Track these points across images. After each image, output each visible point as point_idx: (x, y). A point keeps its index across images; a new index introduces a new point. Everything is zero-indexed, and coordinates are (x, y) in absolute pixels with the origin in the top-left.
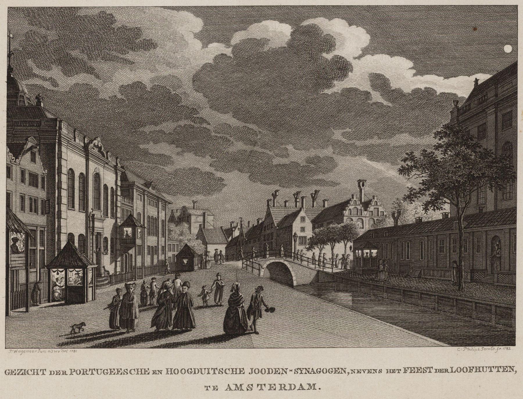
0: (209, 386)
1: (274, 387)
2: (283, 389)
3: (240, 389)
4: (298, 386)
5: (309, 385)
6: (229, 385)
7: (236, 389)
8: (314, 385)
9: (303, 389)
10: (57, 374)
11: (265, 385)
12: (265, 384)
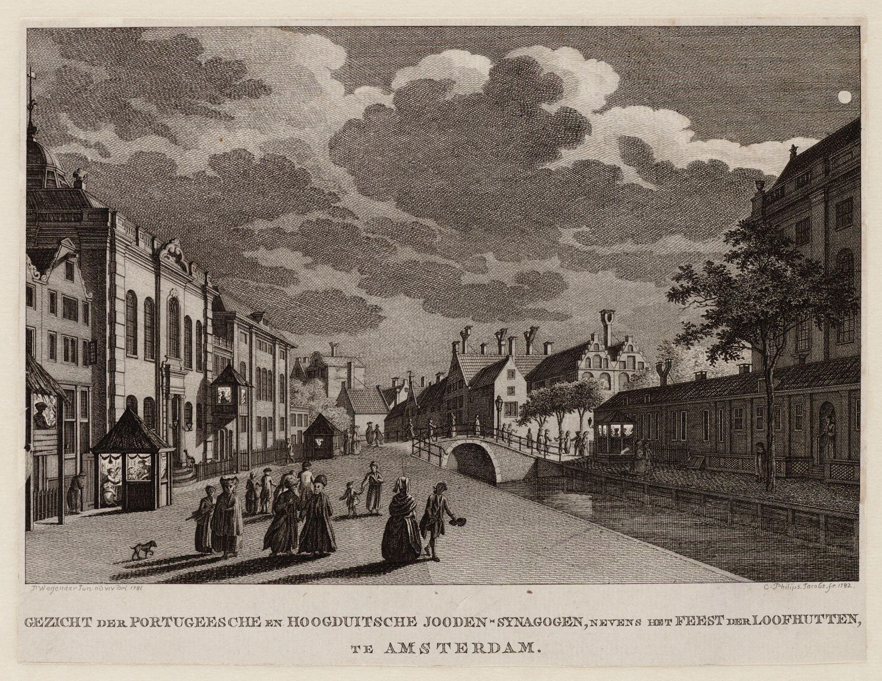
0: (359, 647)
5: (523, 644)
10: (109, 626)
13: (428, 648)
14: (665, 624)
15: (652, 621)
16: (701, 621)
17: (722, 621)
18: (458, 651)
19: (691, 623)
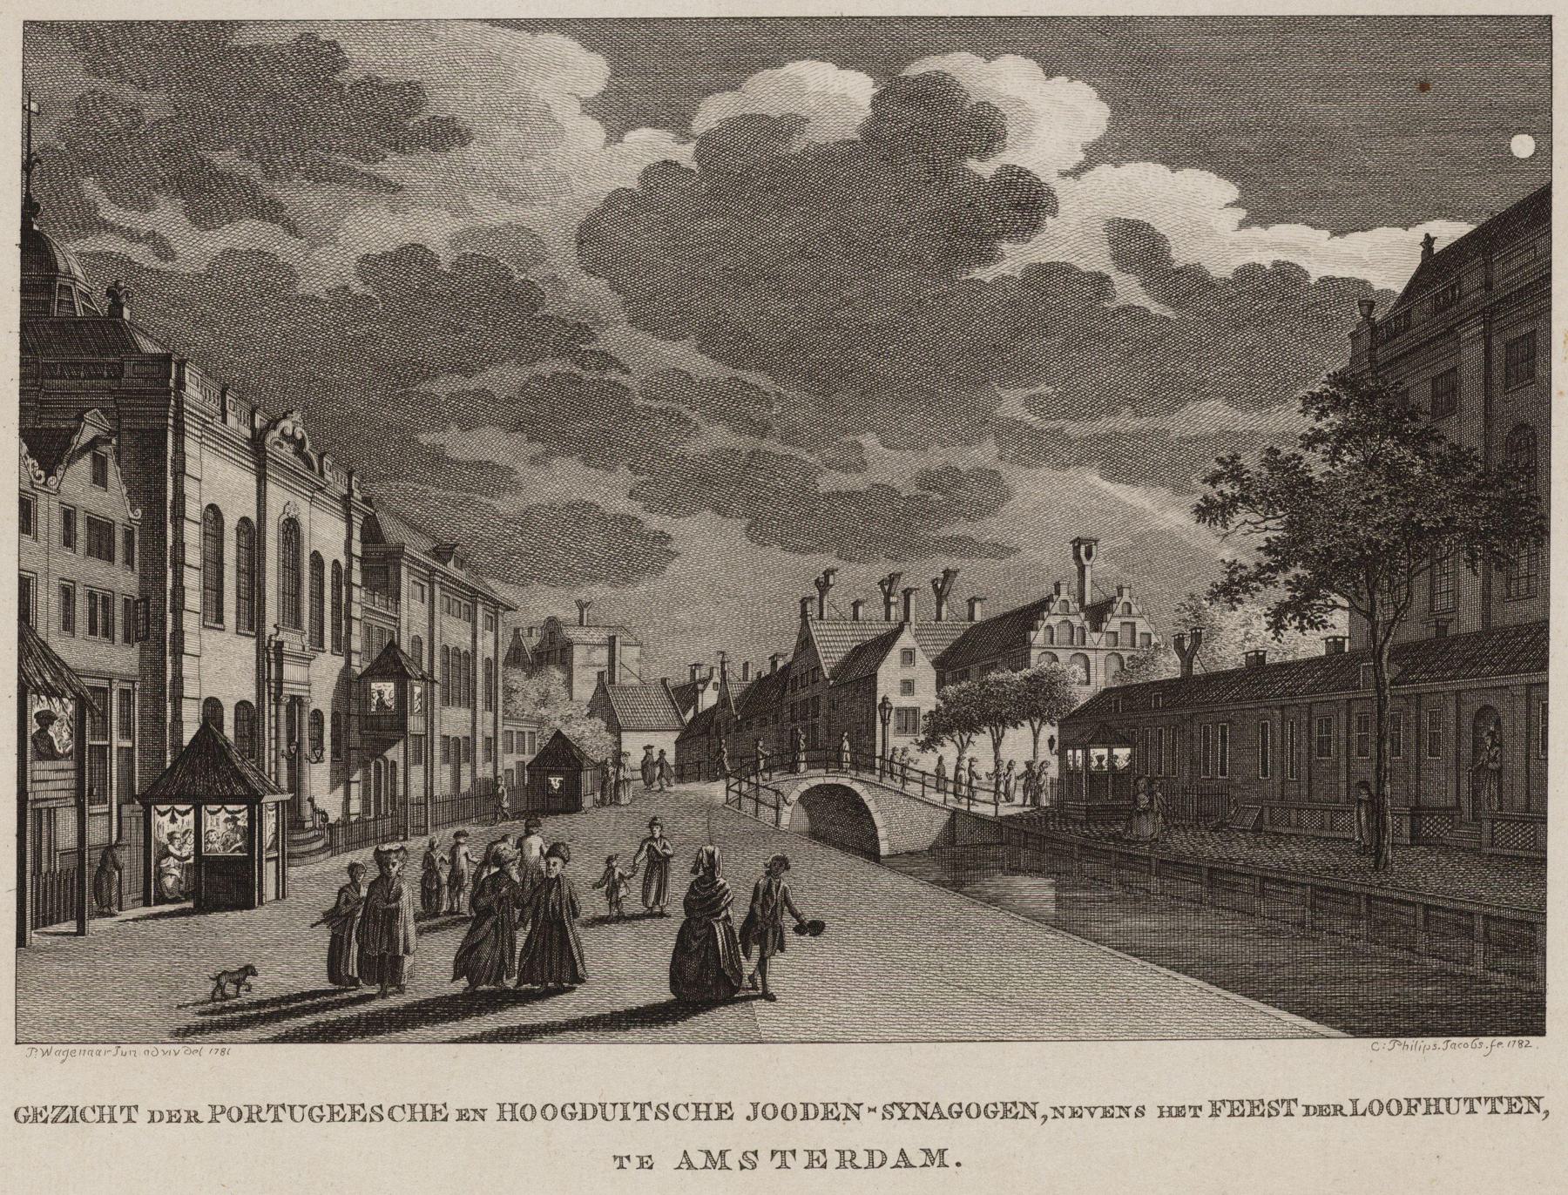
0: (628, 1157)
1: (822, 1160)
2: (848, 1164)
3: (719, 1165)
4: (893, 1157)
5: (927, 1152)
6: (685, 1152)
7: (709, 1165)
8: (942, 1152)
9: (909, 1165)
11: (794, 1152)
12: (794, 1151)
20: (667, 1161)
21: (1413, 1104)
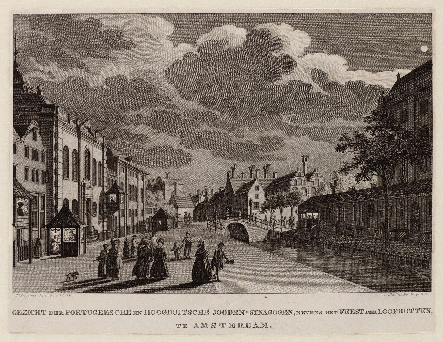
0: (180, 325)
7: (202, 327)
13: (215, 325)
14: (334, 313)
15: (328, 312)
16: (352, 312)
17: (363, 312)
18: (230, 327)
19: (347, 313)
20: (191, 325)
21: (100, 312)
